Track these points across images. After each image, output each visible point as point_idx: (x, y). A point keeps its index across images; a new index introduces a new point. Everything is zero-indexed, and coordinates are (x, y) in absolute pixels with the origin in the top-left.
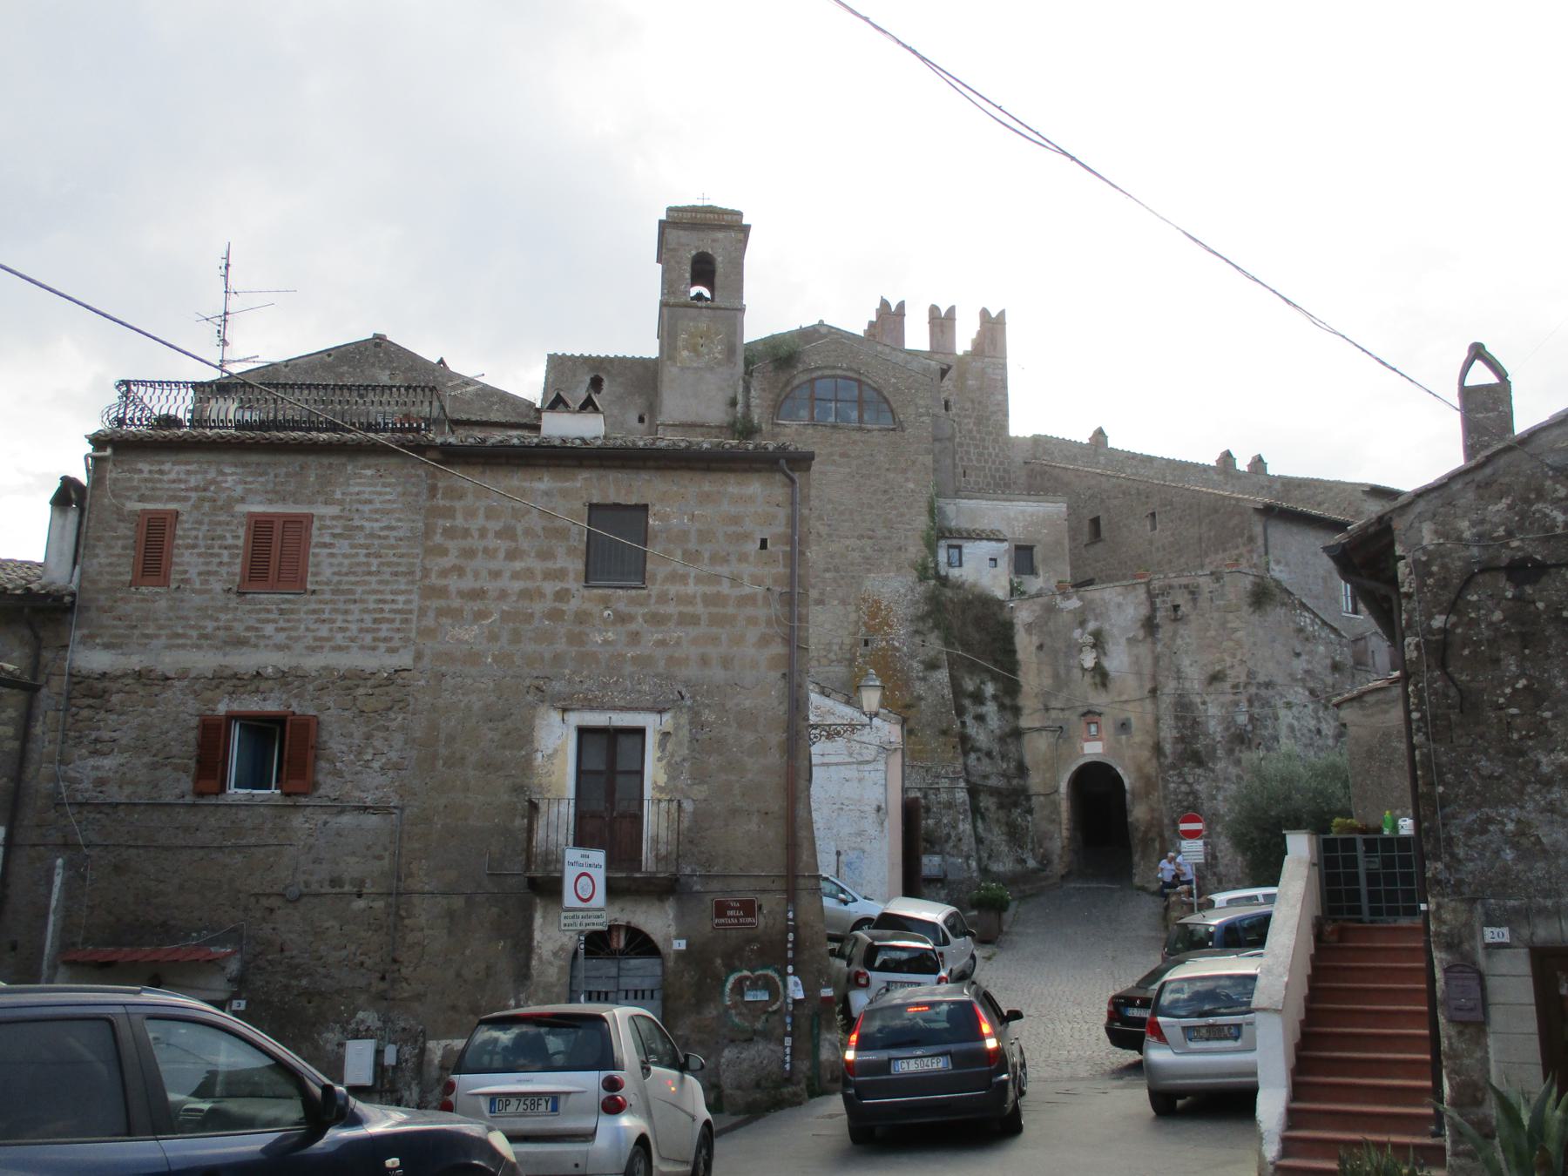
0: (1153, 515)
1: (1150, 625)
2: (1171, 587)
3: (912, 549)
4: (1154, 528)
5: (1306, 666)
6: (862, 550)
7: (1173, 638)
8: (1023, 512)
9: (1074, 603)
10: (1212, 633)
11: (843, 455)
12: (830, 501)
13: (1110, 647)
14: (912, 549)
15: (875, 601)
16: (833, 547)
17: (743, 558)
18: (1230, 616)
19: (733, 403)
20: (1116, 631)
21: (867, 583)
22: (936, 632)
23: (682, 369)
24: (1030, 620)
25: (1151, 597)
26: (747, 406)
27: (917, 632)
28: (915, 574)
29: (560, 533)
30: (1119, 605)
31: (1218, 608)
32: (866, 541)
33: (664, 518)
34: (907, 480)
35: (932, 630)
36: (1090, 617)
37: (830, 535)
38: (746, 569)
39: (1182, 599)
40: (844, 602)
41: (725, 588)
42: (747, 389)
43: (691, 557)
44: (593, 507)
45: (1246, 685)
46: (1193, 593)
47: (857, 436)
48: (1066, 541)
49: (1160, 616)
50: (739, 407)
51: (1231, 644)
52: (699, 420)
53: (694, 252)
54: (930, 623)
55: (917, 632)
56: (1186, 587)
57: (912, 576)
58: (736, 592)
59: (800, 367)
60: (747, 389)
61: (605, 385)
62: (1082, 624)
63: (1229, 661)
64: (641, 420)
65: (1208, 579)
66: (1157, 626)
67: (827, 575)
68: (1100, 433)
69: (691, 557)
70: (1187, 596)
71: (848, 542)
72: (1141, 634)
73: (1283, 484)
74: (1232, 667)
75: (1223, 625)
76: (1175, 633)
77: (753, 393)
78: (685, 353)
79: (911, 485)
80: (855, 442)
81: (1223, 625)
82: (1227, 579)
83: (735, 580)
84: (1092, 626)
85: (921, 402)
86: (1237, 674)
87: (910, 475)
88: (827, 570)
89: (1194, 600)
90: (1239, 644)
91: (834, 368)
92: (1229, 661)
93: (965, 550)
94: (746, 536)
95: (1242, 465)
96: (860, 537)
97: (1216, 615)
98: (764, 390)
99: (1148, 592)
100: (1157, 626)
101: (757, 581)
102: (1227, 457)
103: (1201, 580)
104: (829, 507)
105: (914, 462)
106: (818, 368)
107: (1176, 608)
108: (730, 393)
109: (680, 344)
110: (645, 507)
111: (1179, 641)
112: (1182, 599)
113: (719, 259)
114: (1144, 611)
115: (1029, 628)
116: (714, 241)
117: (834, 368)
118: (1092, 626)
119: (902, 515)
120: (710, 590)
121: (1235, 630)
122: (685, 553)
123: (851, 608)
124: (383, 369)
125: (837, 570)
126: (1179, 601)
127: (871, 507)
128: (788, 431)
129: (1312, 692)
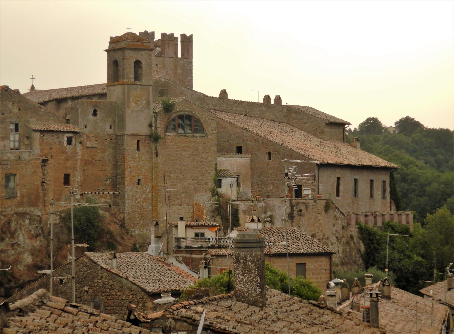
0: (269, 154)
1: (291, 216)
2: (299, 203)
3: (210, 184)
4: (270, 159)
5: (336, 229)
6: (194, 185)
7: (299, 221)
8: (236, 162)
9: (262, 204)
10: (312, 220)
11: (188, 147)
12: (184, 166)
13: (275, 222)
14: (210, 184)
15: (198, 204)
16: (185, 184)
17: (322, 274)
18: (318, 215)
19: (150, 125)
20: (278, 216)
21: (196, 197)
22: (219, 216)
23: (132, 111)
24: (245, 209)
25: (292, 206)
26: (156, 128)
27: (213, 216)
28: (211, 193)
29: (292, 270)
30: (279, 207)
31: (315, 212)
32: (195, 181)
33: (309, 266)
34: (208, 156)
35: (217, 215)
36: (268, 210)
37: (184, 179)
38: (323, 276)
39: (303, 207)
40: (188, 205)
41: (319, 280)
42: (156, 121)
43: (313, 274)
44: (297, 264)
45: (323, 239)
46: (306, 206)
47: (192, 139)
48: (250, 173)
49: (295, 213)
50: (153, 128)
51: (318, 224)
52: (139, 133)
53: (135, 60)
54: (217, 213)
55: (213, 216)
56: (304, 203)
57: (210, 194)
58: (321, 281)
59: (174, 111)
60: (156, 121)
61: (98, 113)
62: (265, 212)
63: (317, 230)
64: (111, 127)
65: (312, 201)
66: (294, 217)
67: (183, 195)
68: (224, 93)
69: (313, 274)
70: (304, 207)
71: (189, 182)
72: (287, 218)
73: (288, 110)
74: (318, 232)
75: (316, 218)
76: (300, 219)
77: (158, 122)
78: (133, 104)
79: (209, 159)
80: (191, 142)
81: (316, 218)
82: (318, 202)
83: (321, 278)
84: (269, 213)
85: (213, 125)
86: (320, 235)
87: (209, 154)
88: (183, 193)
89: (307, 208)
90: (321, 224)
91: (181, 111)
92: (317, 230)
93: (223, 181)
94: (322, 269)
95: (273, 98)
96: (193, 180)
97: (314, 214)
98: (161, 121)
99: (291, 203)
100: (294, 217)
101: (324, 278)
102: (267, 98)
103: (310, 201)
104: (184, 168)
105: (210, 149)
106: (179, 111)
107: (301, 211)
108: (149, 123)
109: (131, 100)
110: (305, 264)
111: (301, 223)
112: (303, 207)
113: (143, 63)
114: (288, 210)
115: (244, 212)
116: (141, 55)
117: (185, 111)
118: (269, 213)
119: (207, 171)
120: (317, 280)
121: (319, 220)
122: (313, 273)
123: (191, 207)
124: (10, 101)
125: (186, 193)
126: (302, 208)
127: (197, 167)
128: (169, 137)
129: (337, 237)
